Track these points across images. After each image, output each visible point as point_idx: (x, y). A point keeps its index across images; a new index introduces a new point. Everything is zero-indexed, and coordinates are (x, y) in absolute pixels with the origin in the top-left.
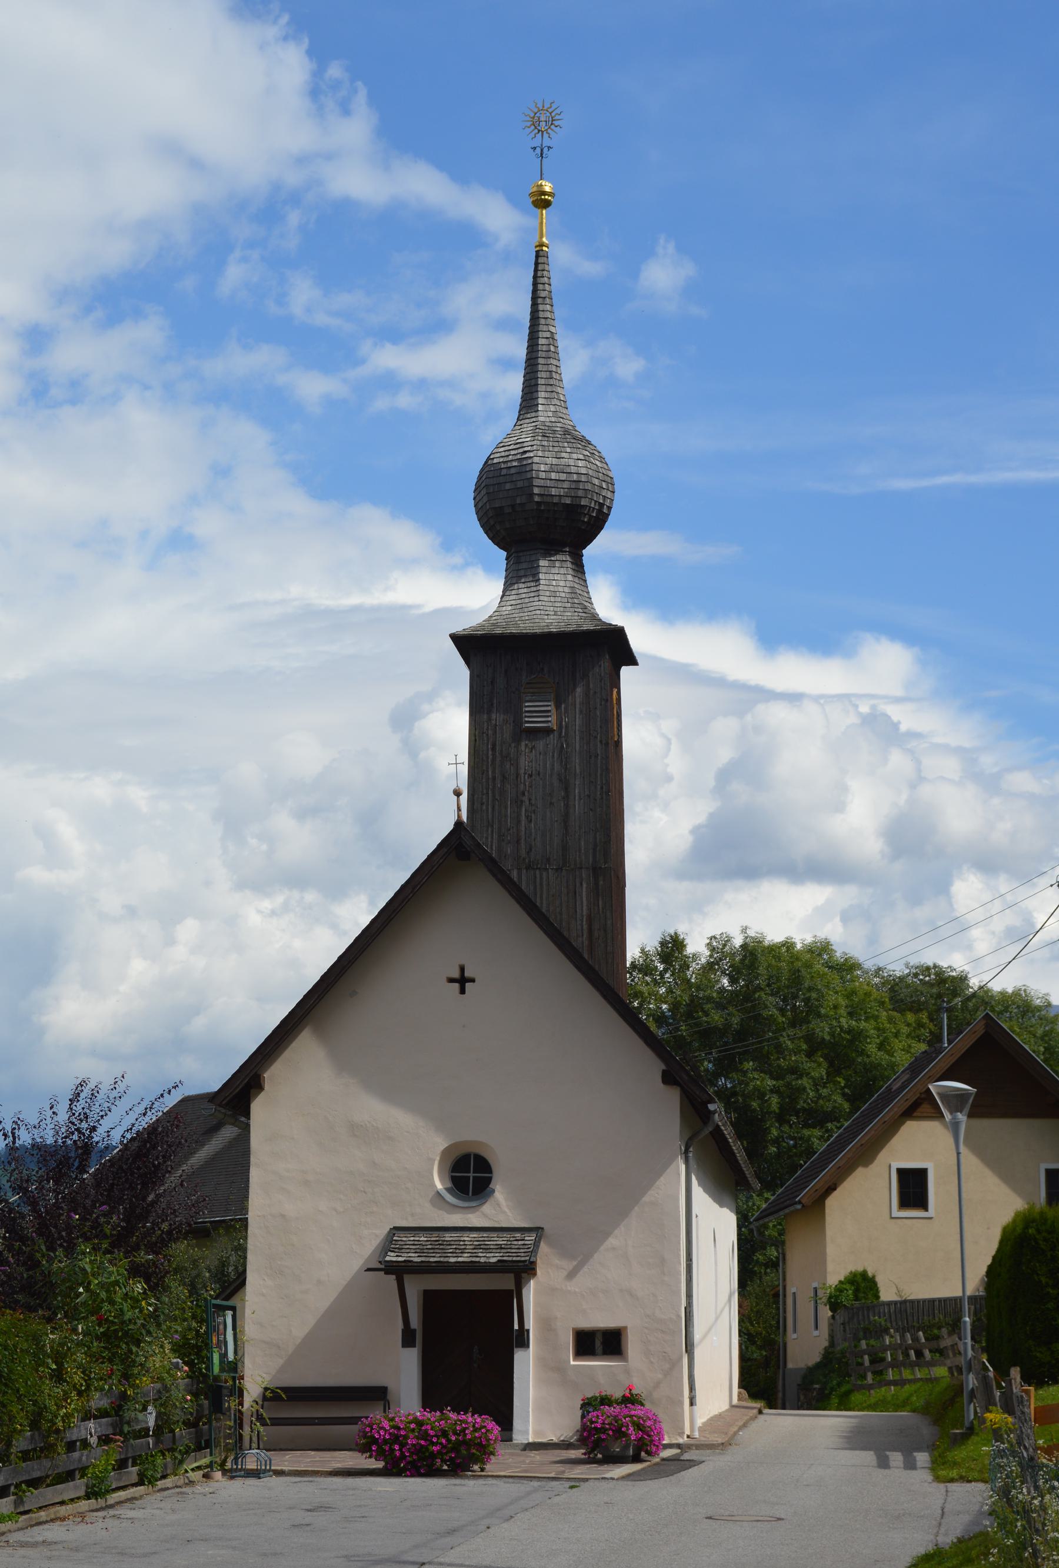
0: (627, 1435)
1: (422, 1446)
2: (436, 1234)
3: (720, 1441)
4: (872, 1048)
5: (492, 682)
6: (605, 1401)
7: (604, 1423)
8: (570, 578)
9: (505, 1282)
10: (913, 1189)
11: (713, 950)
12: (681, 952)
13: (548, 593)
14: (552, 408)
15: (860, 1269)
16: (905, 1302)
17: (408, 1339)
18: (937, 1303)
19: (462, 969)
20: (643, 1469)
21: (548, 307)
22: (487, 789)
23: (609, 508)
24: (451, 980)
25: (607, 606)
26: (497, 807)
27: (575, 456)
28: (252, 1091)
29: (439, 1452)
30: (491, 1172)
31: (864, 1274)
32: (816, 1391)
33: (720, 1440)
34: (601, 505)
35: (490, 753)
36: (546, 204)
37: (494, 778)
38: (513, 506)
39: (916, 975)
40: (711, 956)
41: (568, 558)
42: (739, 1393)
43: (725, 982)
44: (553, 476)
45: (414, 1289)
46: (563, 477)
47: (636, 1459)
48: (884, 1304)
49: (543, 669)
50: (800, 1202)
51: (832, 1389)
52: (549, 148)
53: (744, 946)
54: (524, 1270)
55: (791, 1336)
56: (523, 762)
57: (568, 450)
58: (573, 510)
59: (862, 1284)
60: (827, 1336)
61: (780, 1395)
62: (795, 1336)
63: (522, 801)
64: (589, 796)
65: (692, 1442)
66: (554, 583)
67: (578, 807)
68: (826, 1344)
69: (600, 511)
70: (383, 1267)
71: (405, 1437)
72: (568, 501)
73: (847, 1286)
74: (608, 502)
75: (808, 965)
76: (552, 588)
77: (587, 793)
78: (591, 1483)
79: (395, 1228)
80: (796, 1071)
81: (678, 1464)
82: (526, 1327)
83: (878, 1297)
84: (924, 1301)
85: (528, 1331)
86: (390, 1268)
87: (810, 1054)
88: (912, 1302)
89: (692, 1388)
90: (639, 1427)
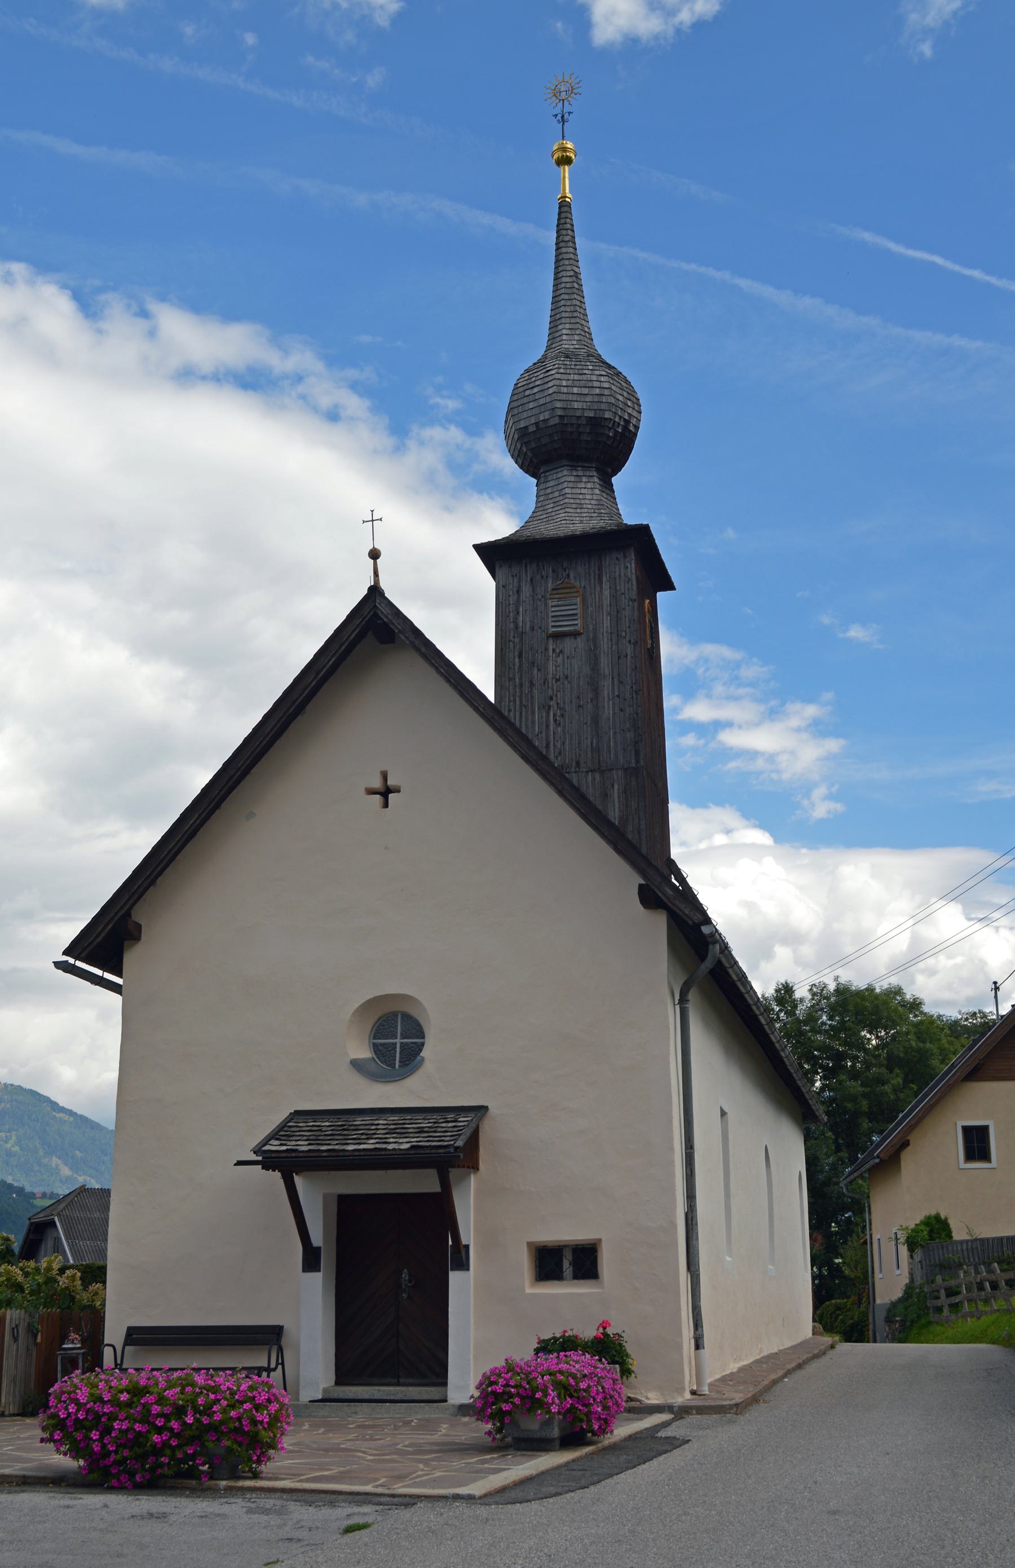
0: (546, 1406)
3: (738, 1398)
4: (935, 1062)
5: (518, 592)
6: (566, 1344)
7: (507, 1385)
8: (597, 491)
9: (427, 1182)
10: (977, 1144)
11: (814, 994)
12: (790, 997)
13: (574, 506)
14: (576, 337)
15: (933, 1213)
16: (976, 1240)
17: (311, 1260)
18: (1005, 1241)
19: (385, 776)
20: (567, 1464)
22: (514, 696)
23: (637, 428)
24: (371, 792)
25: (630, 518)
26: (524, 713)
27: (597, 373)
28: (126, 943)
29: (165, 1444)
30: (423, 1037)
31: (937, 1217)
32: (911, 1320)
33: (760, 1387)
34: (627, 422)
35: (517, 660)
36: (568, 161)
37: (521, 685)
38: (537, 424)
39: (967, 1019)
40: (813, 999)
41: (595, 474)
42: (814, 1328)
44: (575, 390)
46: (586, 391)
47: (571, 1439)
48: (957, 1242)
49: (568, 576)
50: (878, 1157)
51: (912, 1322)
52: (570, 113)
53: (837, 991)
54: (464, 1156)
55: (878, 1275)
56: (551, 667)
57: (591, 367)
58: (596, 423)
59: (937, 1228)
60: (907, 1274)
61: (871, 1327)
62: (881, 1276)
63: (550, 707)
64: (618, 696)
65: (697, 1402)
66: (581, 497)
67: (608, 710)
68: (907, 1281)
69: (626, 428)
71: (112, 1417)
72: (592, 414)
73: (922, 1227)
74: (634, 421)
76: (578, 501)
78: (421, 1515)
79: (297, 1113)
80: (881, 1081)
81: (648, 1447)
82: (464, 1242)
83: (951, 1237)
84: (993, 1239)
85: (467, 1247)
86: (269, 1161)
88: (982, 1240)
89: (698, 1324)
90: (566, 1390)
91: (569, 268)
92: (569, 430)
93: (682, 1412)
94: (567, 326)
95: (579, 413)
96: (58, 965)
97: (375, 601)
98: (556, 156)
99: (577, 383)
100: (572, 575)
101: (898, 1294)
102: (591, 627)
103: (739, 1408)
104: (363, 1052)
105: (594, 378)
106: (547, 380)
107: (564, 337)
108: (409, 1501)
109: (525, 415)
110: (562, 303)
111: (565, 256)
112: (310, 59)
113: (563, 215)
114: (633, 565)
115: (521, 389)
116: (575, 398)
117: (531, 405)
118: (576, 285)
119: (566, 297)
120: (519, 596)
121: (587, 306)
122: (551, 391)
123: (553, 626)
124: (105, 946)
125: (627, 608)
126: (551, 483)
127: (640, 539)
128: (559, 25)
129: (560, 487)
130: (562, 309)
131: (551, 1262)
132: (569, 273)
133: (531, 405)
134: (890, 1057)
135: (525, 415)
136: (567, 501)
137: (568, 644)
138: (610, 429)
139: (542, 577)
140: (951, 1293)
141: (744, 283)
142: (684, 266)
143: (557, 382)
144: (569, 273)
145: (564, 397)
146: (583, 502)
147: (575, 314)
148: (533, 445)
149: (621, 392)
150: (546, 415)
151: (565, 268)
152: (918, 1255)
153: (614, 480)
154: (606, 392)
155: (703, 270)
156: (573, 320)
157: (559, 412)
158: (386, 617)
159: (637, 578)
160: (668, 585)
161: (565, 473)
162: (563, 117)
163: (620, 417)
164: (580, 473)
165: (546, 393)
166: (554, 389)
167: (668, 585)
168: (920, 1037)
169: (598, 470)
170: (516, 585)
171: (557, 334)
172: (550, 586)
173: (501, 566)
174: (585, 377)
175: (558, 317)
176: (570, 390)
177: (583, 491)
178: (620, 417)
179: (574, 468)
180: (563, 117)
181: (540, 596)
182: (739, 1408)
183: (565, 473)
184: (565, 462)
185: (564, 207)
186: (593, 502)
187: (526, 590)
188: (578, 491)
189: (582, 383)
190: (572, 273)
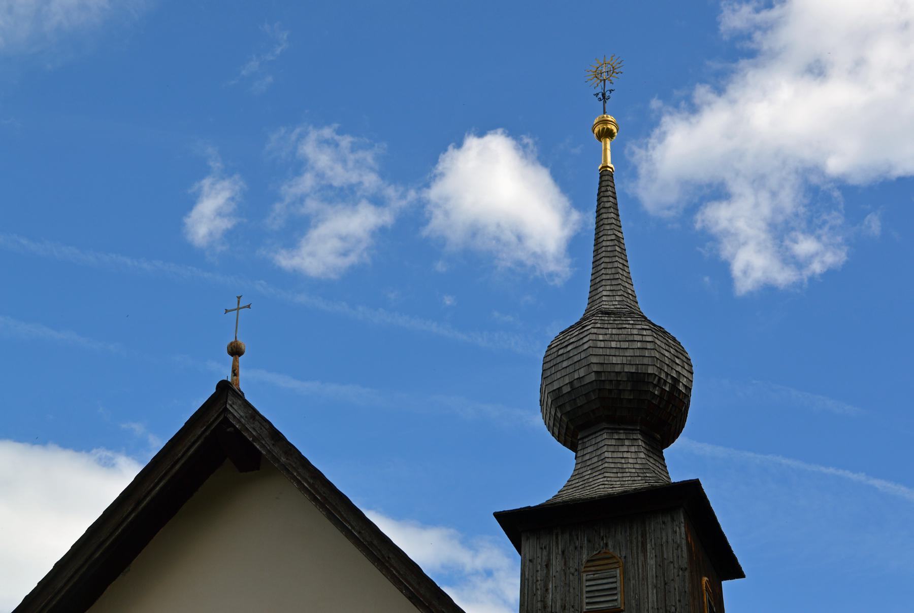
5: (547, 566)
14: (618, 298)
23: (689, 389)
34: (676, 381)
36: (609, 134)
38: (571, 383)
41: (639, 436)
44: (613, 344)
46: (625, 345)
49: (606, 545)
52: (611, 91)
58: (639, 379)
66: (623, 461)
74: (684, 381)
91: (610, 232)
92: (608, 387)
94: (608, 288)
95: (618, 369)
97: (226, 403)
98: (596, 130)
99: (616, 338)
100: (610, 544)
102: (633, 602)
105: (635, 332)
106: (581, 336)
107: (604, 298)
109: (559, 375)
110: (603, 266)
111: (606, 221)
112: (496, 314)
113: (604, 184)
114: (683, 529)
115: (555, 350)
116: (613, 352)
117: (565, 364)
118: (617, 249)
119: (607, 260)
120: (548, 570)
121: (631, 270)
122: (586, 346)
123: (588, 603)
125: (677, 578)
126: (590, 450)
127: (690, 499)
128: (707, 279)
129: (599, 452)
130: (603, 271)
132: (609, 238)
133: (565, 364)
135: (559, 375)
136: (606, 465)
138: (655, 386)
139: (576, 548)
141: (878, 483)
142: (824, 470)
143: (594, 337)
144: (609, 238)
145: (601, 352)
146: (625, 466)
147: (617, 276)
148: (568, 408)
149: (667, 348)
150: (582, 373)
151: (605, 232)
153: (666, 452)
154: (649, 346)
155: (840, 472)
156: (614, 282)
157: (595, 368)
158: (239, 421)
159: (688, 544)
160: (736, 572)
161: (605, 436)
162: (603, 95)
163: (667, 374)
164: (622, 436)
165: (581, 349)
166: (590, 343)
167: (736, 572)
169: (642, 433)
170: (544, 558)
171: (597, 297)
172: (585, 557)
173: (528, 538)
174: (625, 331)
175: (598, 280)
176: (608, 344)
177: (625, 455)
178: (667, 374)
179: (615, 430)
180: (603, 95)
181: (572, 570)
183: (605, 436)
184: (605, 425)
185: (606, 176)
186: (637, 466)
187: (557, 565)
188: (620, 455)
189: (621, 338)
190: (613, 237)
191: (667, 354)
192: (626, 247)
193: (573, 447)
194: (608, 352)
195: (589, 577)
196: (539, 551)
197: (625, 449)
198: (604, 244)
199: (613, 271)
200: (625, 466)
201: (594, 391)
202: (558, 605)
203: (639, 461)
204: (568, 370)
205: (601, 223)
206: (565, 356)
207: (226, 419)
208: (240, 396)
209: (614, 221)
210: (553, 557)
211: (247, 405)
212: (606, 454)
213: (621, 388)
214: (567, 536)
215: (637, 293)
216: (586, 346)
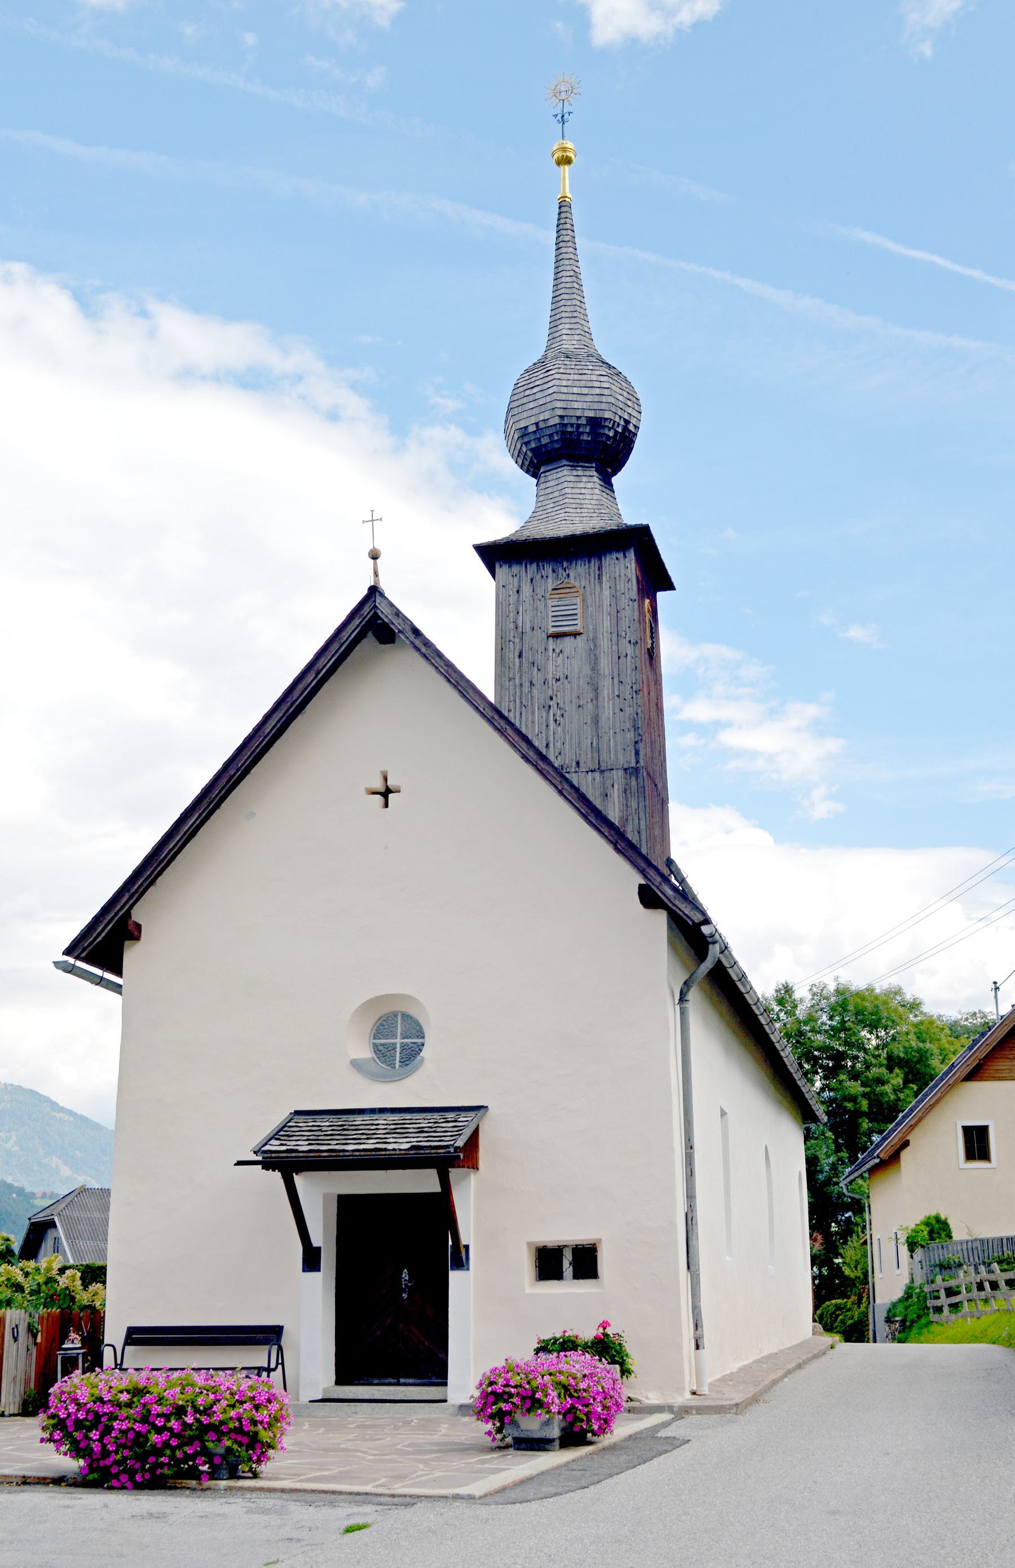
1: (138, 1434)
2: (344, 1117)
3: (738, 1398)
5: (518, 592)
6: (567, 1345)
7: (507, 1385)
8: (597, 491)
9: (423, 1182)
10: (977, 1143)
14: (577, 337)
15: (933, 1213)
17: (311, 1260)
21: (568, 226)
22: (514, 695)
23: (636, 427)
25: (630, 518)
28: (127, 943)
33: (758, 1390)
34: (627, 422)
36: (568, 161)
38: (537, 424)
39: (967, 1019)
41: (595, 474)
43: (824, 1018)
44: (576, 390)
45: (318, 1193)
46: (585, 391)
48: (956, 1242)
49: (568, 575)
52: (569, 113)
53: (838, 992)
56: (551, 668)
57: (591, 367)
59: (938, 1229)
61: (871, 1327)
62: (881, 1276)
65: (696, 1401)
66: (581, 496)
67: (608, 710)
69: (626, 428)
70: (260, 1158)
74: (634, 421)
75: (885, 1003)
77: (617, 693)
79: (297, 1113)
80: (880, 1081)
81: (648, 1447)
85: (467, 1247)
86: (269, 1162)
87: (890, 1069)
90: (566, 1389)
91: (569, 268)
93: (682, 1412)
95: (579, 413)
96: (57, 964)
98: (556, 156)
99: (577, 383)
100: (571, 575)
101: (900, 1294)
103: (738, 1408)
104: (364, 1052)
105: (594, 378)
106: (547, 379)
108: (410, 1501)
111: (565, 256)
113: (563, 215)
116: (575, 398)
117: (531, 405)
118: (576, 285)
122: (551, 391)
124: (105, 945)
125: (627, 608)
127: (639, 541)
131: (548, 1263)
133: (531, 405)
134: (890, 1058)
136: (567, 501)
137: (568, 643)
138: (610, 429)
140: (950, 1292)
146: (583, 502)
147: (575, 314)
149: (621, 392)
150: (547, 415)
152: (919, 1253)
153: (614, 480)
154: (606, 392)
156: (573, 320)
161: (565, 472)
163: (620, 417)
164: (580, 473)
165: (546, 393)
167: (669, 586)
168: (919, 1038)
175: (558, 317)
176: (570, 390)
177: (583, 491)
178: (620, 417)
181: (540, 597)
182: (738, 1408)
184: (564, 462)
185: (564, 206)
186: (593, 502)
187: (526, 590)
188: (578, 491)
189: (582, 384)
190: (572, 273)
191: (621, 398)
192: (583, 282)
193: (535, 475)
194: (570, 397)
195: (554, 604)
196: (511, 578)
197: (582, 485)
198: (564, 280)
199: (572, 308)
200: (583, 502)
201: (557, 433)
202: (528, 626)
203: (595, 497)
204: (535, 411)
205: (560, 257)
206: (531, 398)
207: (376, 614)
208: (382, 595)
209: (572, 256)
210: (523, 585)
211: (391, 605)
212: (567, 490)
213: (581, 430)
214: (534, 566)
215: (592, 331)
216: (551, 391)
